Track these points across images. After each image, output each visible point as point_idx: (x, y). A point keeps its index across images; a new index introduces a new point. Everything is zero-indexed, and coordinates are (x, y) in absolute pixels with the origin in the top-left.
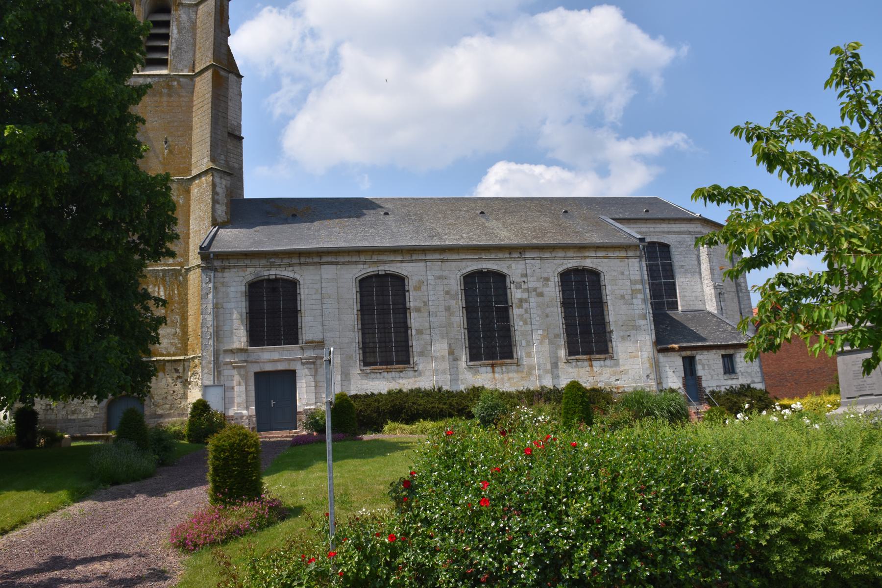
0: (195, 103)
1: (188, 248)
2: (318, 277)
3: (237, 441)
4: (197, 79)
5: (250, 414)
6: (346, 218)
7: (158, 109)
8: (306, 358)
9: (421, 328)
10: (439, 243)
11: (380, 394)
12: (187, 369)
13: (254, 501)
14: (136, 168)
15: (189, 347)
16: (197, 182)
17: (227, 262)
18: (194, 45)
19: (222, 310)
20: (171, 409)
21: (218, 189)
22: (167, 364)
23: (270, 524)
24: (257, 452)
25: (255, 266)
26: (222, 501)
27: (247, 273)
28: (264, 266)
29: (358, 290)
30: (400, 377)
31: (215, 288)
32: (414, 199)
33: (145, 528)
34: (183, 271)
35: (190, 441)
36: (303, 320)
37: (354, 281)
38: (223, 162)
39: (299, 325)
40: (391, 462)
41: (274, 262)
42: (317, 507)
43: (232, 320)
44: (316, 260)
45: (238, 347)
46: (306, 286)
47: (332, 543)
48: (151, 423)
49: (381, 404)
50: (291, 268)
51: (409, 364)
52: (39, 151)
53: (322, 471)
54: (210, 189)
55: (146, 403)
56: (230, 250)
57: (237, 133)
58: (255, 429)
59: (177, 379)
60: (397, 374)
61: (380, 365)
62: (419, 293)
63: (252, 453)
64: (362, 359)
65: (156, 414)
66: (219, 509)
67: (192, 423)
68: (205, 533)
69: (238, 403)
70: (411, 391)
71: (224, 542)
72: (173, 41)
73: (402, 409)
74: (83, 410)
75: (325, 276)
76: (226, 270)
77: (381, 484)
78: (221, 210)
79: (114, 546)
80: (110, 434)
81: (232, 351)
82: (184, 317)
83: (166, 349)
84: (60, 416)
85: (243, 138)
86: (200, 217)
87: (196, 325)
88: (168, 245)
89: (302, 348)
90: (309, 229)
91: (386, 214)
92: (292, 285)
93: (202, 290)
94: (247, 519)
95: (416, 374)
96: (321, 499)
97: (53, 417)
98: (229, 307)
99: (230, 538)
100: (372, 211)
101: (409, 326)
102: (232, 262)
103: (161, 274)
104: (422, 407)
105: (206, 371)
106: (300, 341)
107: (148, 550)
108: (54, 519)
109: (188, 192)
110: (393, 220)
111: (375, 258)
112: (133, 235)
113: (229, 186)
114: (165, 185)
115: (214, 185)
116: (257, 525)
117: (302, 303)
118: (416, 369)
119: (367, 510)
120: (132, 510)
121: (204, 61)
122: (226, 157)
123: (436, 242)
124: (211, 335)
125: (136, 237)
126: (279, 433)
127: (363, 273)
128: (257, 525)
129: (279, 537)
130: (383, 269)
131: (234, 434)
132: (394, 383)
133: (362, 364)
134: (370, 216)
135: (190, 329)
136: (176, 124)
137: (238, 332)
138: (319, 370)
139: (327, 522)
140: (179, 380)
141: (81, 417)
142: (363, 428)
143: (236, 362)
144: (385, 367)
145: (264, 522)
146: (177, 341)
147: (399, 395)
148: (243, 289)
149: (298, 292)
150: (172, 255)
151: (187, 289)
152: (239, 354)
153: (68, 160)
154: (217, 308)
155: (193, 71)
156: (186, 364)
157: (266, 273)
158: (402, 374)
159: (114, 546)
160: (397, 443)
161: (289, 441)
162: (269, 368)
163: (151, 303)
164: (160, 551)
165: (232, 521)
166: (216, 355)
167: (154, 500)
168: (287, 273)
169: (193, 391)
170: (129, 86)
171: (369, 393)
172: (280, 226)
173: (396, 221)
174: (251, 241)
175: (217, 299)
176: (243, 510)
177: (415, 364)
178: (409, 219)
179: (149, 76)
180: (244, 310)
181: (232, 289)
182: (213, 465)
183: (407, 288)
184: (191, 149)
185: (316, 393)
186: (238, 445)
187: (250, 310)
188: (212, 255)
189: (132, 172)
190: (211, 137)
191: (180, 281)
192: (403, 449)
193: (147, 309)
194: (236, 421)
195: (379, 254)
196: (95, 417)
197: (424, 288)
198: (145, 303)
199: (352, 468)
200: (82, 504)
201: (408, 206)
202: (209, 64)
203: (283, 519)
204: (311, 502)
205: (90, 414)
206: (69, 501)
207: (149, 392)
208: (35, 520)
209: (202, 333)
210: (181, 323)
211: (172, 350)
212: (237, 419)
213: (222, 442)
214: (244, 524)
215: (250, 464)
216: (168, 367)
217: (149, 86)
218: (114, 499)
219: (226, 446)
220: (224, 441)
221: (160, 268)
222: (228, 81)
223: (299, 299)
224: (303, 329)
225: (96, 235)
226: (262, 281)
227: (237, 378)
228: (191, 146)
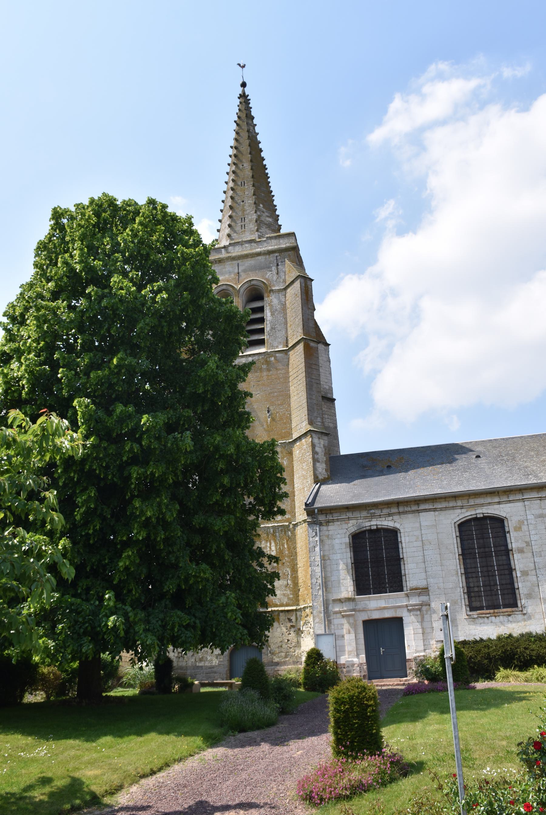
0: (290, 374)
1: (294, 505)
2: (417, 525)
3: (356, 694)
4: (291, 353)
5: (361, 662)
6: (438, 464)
7: (260, 383)
8: (412, 605)
9: (526, 569)
10: (535, 481)
11: (489, 639)
12: (299, 618)
13: (375, 755)
14: (246, 438)
15: (300, 598)
16: (298, 444)
17: (331, 516)
18: (286, 323)
19: (328, 561)
20: (286, 657)
21: (317, 449)
22: (281, 614)
23: (393, 780)
24: (376, 704)
25: (356, 519)
26: (344, 754)
27: (350, 525)
28: (365, 518)
29: (458, 534)
30: (509, 621)
31: (321, 541)
32: (503, 439)
33: (272, 778)
34: (291, 526)
35: (306, 689)
36: (406, 568)
37: (453, 526)
38: (319, 424)
39: (403, 572)
40: (510, 715)
41: (374, 513)
42: (439, 763)
43: (338, 570)
44: (414, 508)
45: (346, 596)
46: (406, 534)
47: (463, 809)
48: (269, 670)
49: (491, 650)
50: (391, 518)
51: (517, 606)
52: (168, 434)
53: (439, 724)
54: (310, 449)
55: (263, 651)
56: (332, 504)
57: (329, 396)
58: (367, 677)
59: (290, 628)
60: (505, 618)
61: (487, 609)
62: (520, 534)
63: (370, 706)
64: (467, 603)
65: (272, 662)
66: (341, 762)
67: (306, 671)
68: (330, 786)
69: (349, 652)
70: (522, 635)
71: (348, 798)
72: (268, 322)
73: (514, 655)
74: (209, 658)
75: (423, 524)
76: (330, 524)
77: (503, 739)
78: (322, 468)
79: (246, 794)
80: (233, 681)
81: (340, 601)
82: (294, 570)
83: (280, 599)
84: (190, 664)
85: (335, 400)
86: (303, 476)
87: (306, 576)
88: (278, 503)
89: (407, 595)
90: (405, 478)
91: (478, 457)
92: (393, 533)
93: (309, 543)
94: (370, 774)
95: (525, 617)
96: (442, 755)
97: (184, 664)
98: (335, 558)
99: (354, 794)
100: (463, 456)
101: (513, 568)
102: (336, 516)
103: (272, 530)
104: (535, 652)
105: (317, 620)
106: (405, 589)
107: (277, 801)
108: (192, 763)
109: (291, 453)
110: (486, 463)
111: (472, 502)
112: (249, 497)
113: (326, 445)
114: (272, 450)
115: (313, 446)
116: (380, 781)
117: (404, 551)
118: (525, 612)
119: (492, 769)
120: (259, 758)
121: (295, 336)
122: (322, 418)
123: (532, 481)
124: (320, 585)
125: (252, 499)
126: (390, 681)
127: (461, 517)
128: (380, 781)
129: (403, 795)
130: (480, 512)
131: (353, 687)
132: (502, 627)
133: (468, 609)
134: (462, 460)
135: (300, 581)
136: (276, 394)
137: (345, 581)
138: (425, 616)
139: (455, 784)
140: (293, 629)
141: (207, 664)
142: (474, 675)
143: (345, 611)
144: (492, 611)
145: (387, 778)
146: (289, 592)
147: (509, 640)
148: (347, 540)
149: (399, 540)
150: (282, 512)
151: (295, 543)
152: (347, 603)
153: (193, 440)
154: (324, 560)
155: (287, 346)
156: (298, 613)
157: (368, 524)
158: (510, 618)
159: (246, 794)
160: (514, 692)
161: (401, 690)
162: (376, 615)
163: (265, 561)
164: (289, 803)
165: (355, 775)
166: (326, 605)
167: (278, 749)
168: (388, 523)
169: (305, 639)
170: (235, 365)
171: (478, 639)
172: (377, 478)
173: (488, 463)
174: (351, 494)
175: (323, 551)
176: (365, 764)
177: (523, 607)
178: (502, 460)
179: (250, 355)
180: (349, 561)
181: (337, 541)
182: (334, 717)
183: (507, 529)
184: (290, 415)
185: (424, 640)
186: (358, 697)
187: (354, 560)
188: (316, 510)
189: (243, 442)
190: (307, 402)
191: (289, 536)
192: (521, 699)
193: (261, 565)
194: (348, 669)
195: (475, 498)
196: (219, 665)
197: (525, 528)
198: (260, 560)
199: (469, 720)
200: (215, 750)
201: (499, 446)
202: (300, 338)
203: (405, 775)
204: (431, 758)
205: (215, 662)
206: (203, 746)
207: (267, 641)
208: (177, 763)
209: (312, 584)
210: (292, 575)
211: (285, 601)
212: (348, 667)
213: (341, 695)
214: (367, 779)
215: (369, 717)
216: (282, 617)
217: (253, 363)
218: (243, 746)
219: (346, 699)
220: (344, 693)
221: (270, 525)
222: (318, 351)
223: (400, 547)
224: (407, 576)
225: (217, 500)
226: (364, 532)
227: (346, 626)
228: (291, 412)
